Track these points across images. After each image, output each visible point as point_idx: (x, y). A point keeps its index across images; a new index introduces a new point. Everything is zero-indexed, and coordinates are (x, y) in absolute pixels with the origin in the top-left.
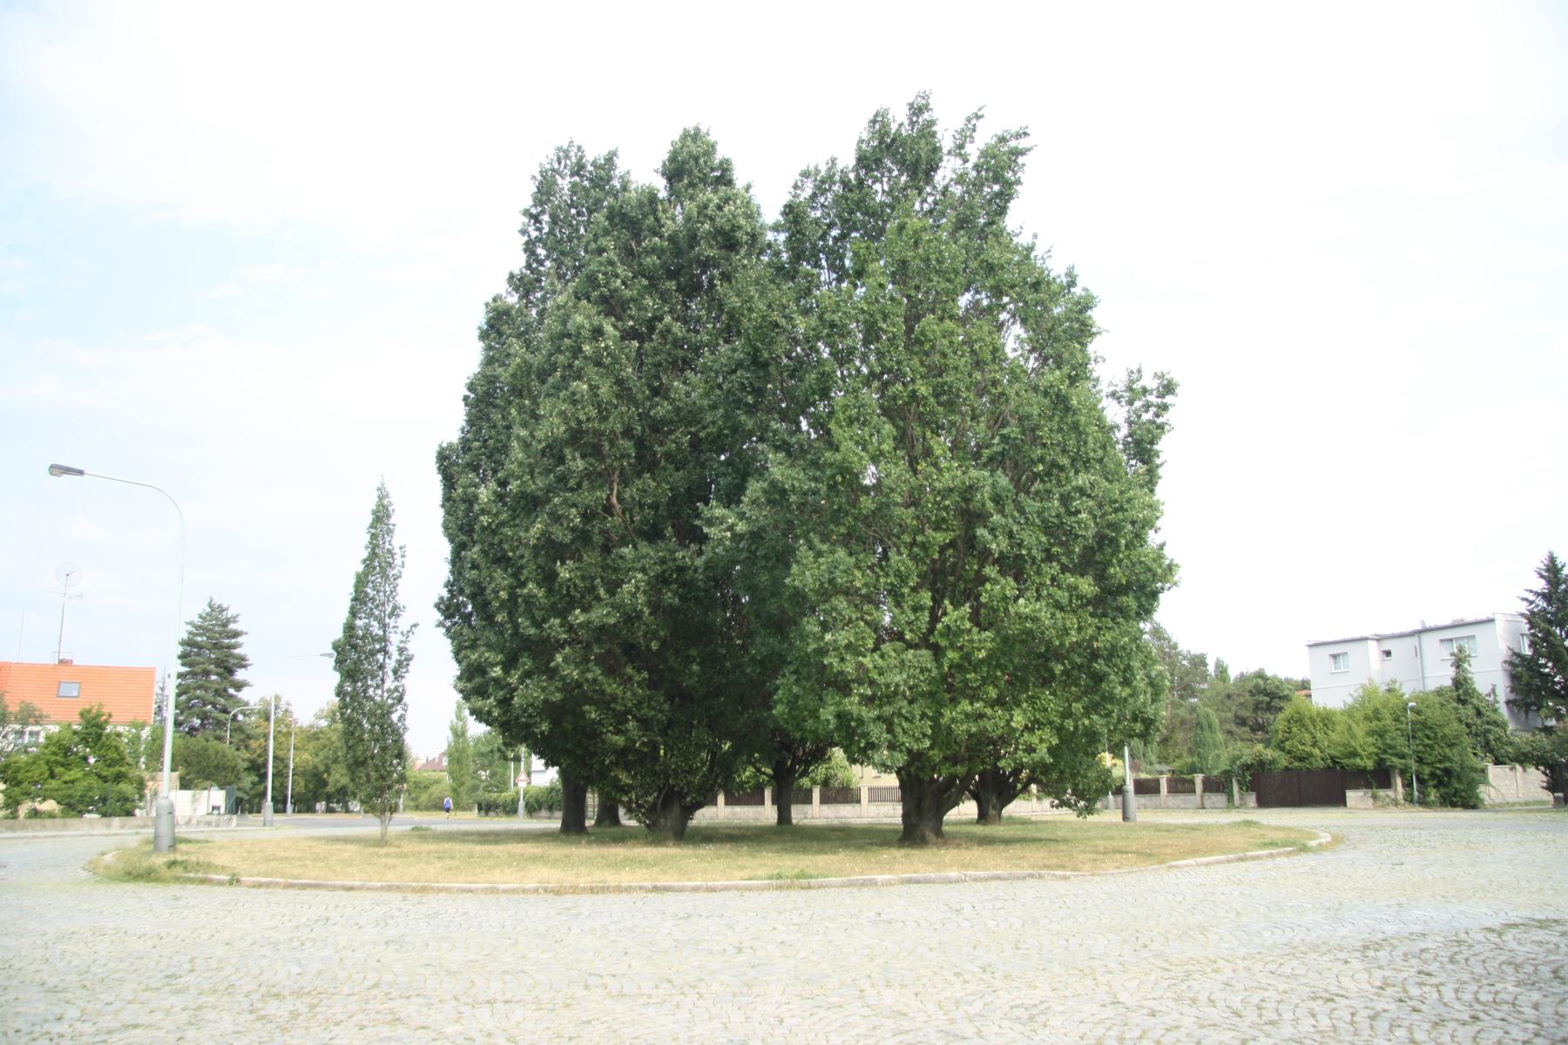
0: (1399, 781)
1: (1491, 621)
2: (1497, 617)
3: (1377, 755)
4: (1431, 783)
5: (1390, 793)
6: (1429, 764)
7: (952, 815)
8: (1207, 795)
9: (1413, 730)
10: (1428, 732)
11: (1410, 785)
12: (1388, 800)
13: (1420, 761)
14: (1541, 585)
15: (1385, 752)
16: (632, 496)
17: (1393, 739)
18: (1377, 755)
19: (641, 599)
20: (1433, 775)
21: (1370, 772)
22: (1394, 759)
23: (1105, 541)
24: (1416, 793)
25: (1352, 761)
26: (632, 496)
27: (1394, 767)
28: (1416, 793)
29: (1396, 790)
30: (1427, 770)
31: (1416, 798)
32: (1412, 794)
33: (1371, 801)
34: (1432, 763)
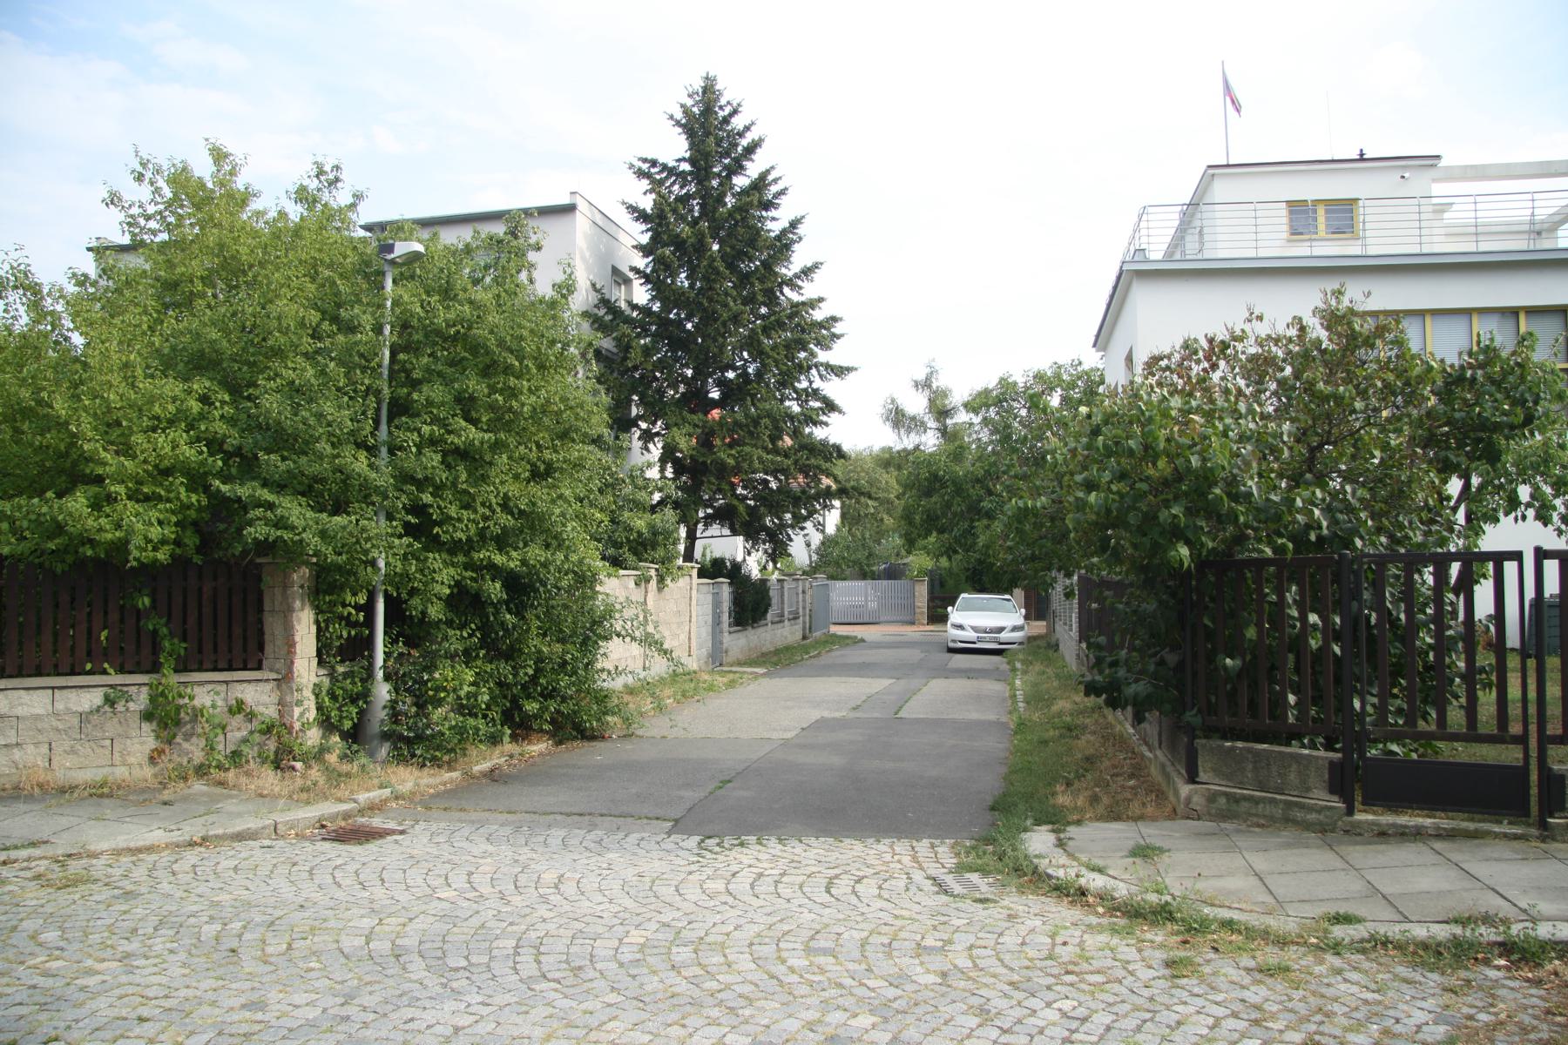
0: (305, 628)
1: (569, 209)
2: (582, 206)
3: (197, 480)
4: (455, 640)
5: (257, 694)
6: (454, 548)
7: (658, 305)
8: (1283, 211)
9: (399, 373)
10: (474, 385)
11: (358, 648)
12: (238, 730)
13: (421, 527)
14: (674, 148)
15: (245, 464)
16: (795, 479)
17: (295, 391)
18: (197, 480)
19: (938, 506)
20: (464, 602)
21: (149, 572)
22: (295, 510)
23: (454, 253)
24: (383, 691)
25: (47, 506)
26: (795, 479)
27: (292, 553)
28: (383, 691)
29: (285, 679)
30: (444, 575)
31: (379, 715)
32: (363, 696)
33: (144, 740)
34: (467, 547)
